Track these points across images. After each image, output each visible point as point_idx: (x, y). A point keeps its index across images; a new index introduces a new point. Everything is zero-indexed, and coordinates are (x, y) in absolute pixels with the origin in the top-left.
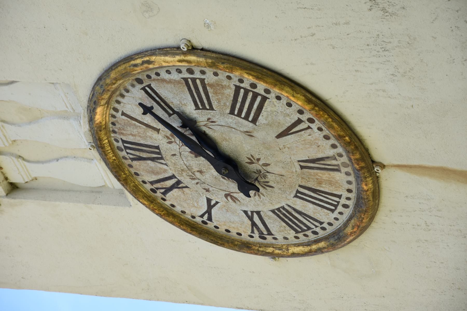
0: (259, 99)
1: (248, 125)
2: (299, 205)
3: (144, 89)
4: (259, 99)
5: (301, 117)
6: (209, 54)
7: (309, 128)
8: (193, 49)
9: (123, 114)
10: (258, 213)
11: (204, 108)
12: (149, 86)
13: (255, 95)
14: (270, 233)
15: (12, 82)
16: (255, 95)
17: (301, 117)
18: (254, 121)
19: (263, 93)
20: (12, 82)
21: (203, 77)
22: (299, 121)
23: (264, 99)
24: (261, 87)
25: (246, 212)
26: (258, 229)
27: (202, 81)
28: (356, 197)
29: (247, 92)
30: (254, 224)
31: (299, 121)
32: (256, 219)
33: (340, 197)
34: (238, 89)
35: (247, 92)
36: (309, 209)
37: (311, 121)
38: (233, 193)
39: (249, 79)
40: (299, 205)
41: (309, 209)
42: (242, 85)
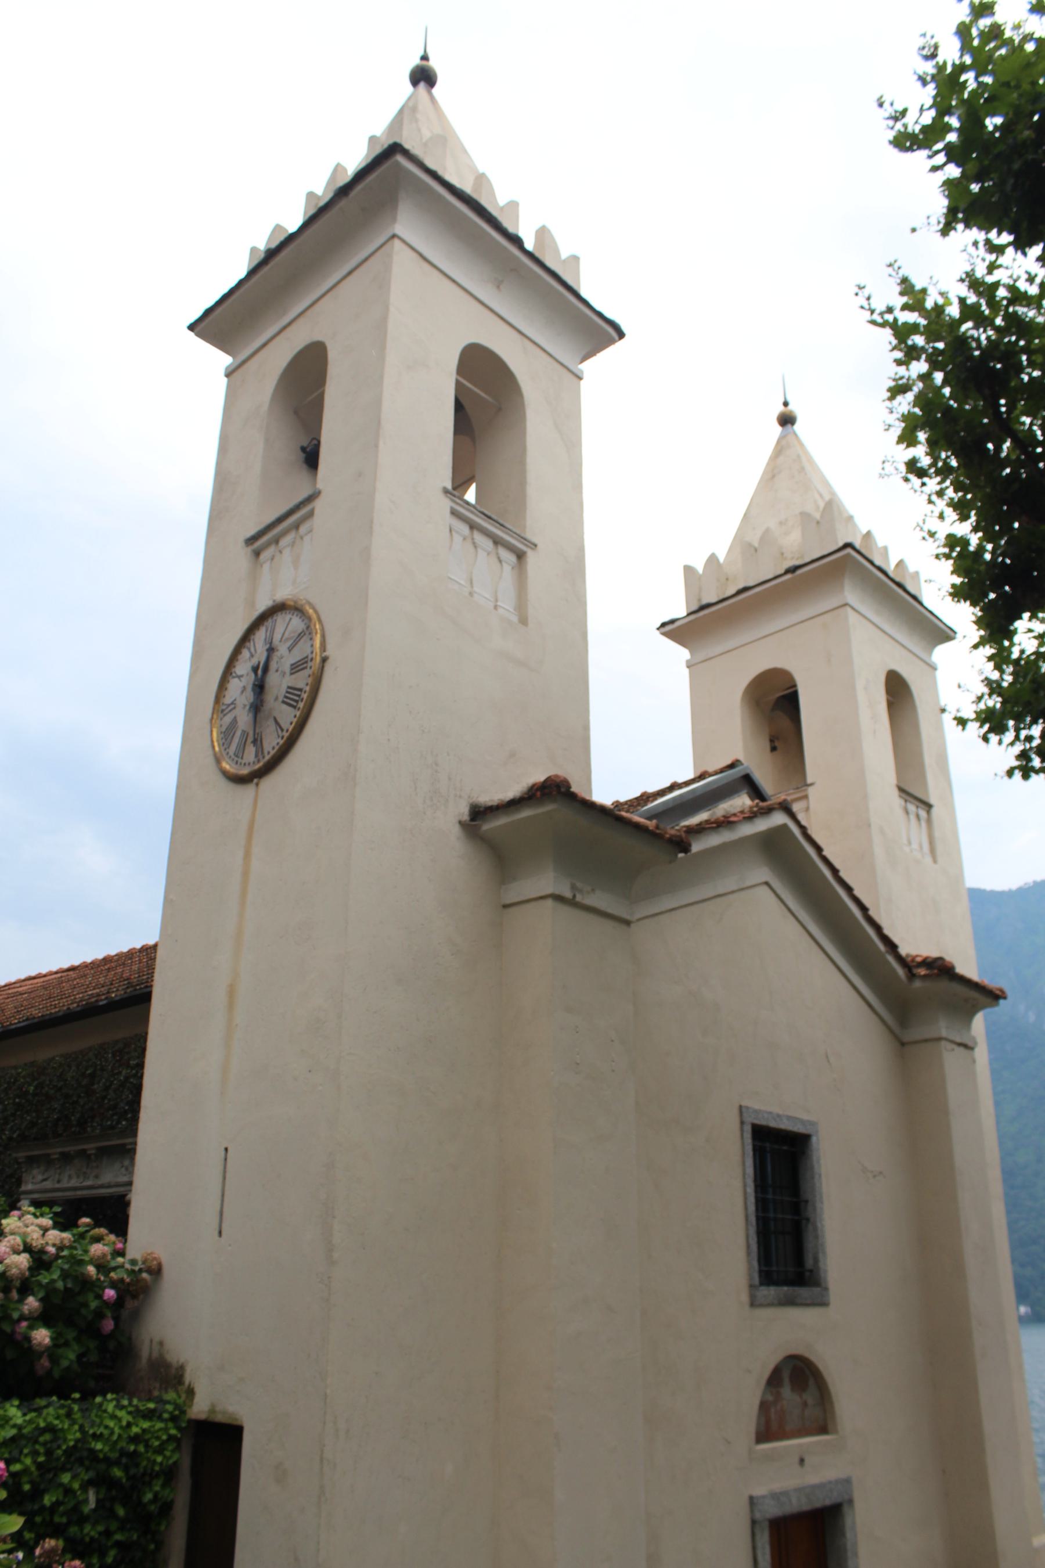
0: (295, 704)
1: (281, 699)
2: (238, 733)
3: (303, 631)
4: (295, 704)
5: (285, 731)
6: (320, 671)
7: (279, 736)
8: (324, 660)
9: (291, 619)
10: (234, 708)
11: (292, 669)
12: (305, 634)
13: (297, 701)
14: (225, 715)
15: (426, 29)
16: (297, 701)
17: (285, 731)
18: (284, 702)
19: (298, 706)
20: (426, 29)
21: (308, 668)
22: (282, 730)
23: (294, 707)
24: (301, 705)
25: (235, 700)
26: (227, 708)
27: (306, 668)
28: (71, 1149)
29: (299, 696)
30: (229, 705)
31: (282, 730)
32: (233, 706)
33: (242, 758)
34: (300, 690)
35: (299, 696)
36: (236, 740)
37: (283, 737)
38: (513, 613)
39: (305, 696)
40: (238, 733)
41: (236, 740)
42: (303, 693)
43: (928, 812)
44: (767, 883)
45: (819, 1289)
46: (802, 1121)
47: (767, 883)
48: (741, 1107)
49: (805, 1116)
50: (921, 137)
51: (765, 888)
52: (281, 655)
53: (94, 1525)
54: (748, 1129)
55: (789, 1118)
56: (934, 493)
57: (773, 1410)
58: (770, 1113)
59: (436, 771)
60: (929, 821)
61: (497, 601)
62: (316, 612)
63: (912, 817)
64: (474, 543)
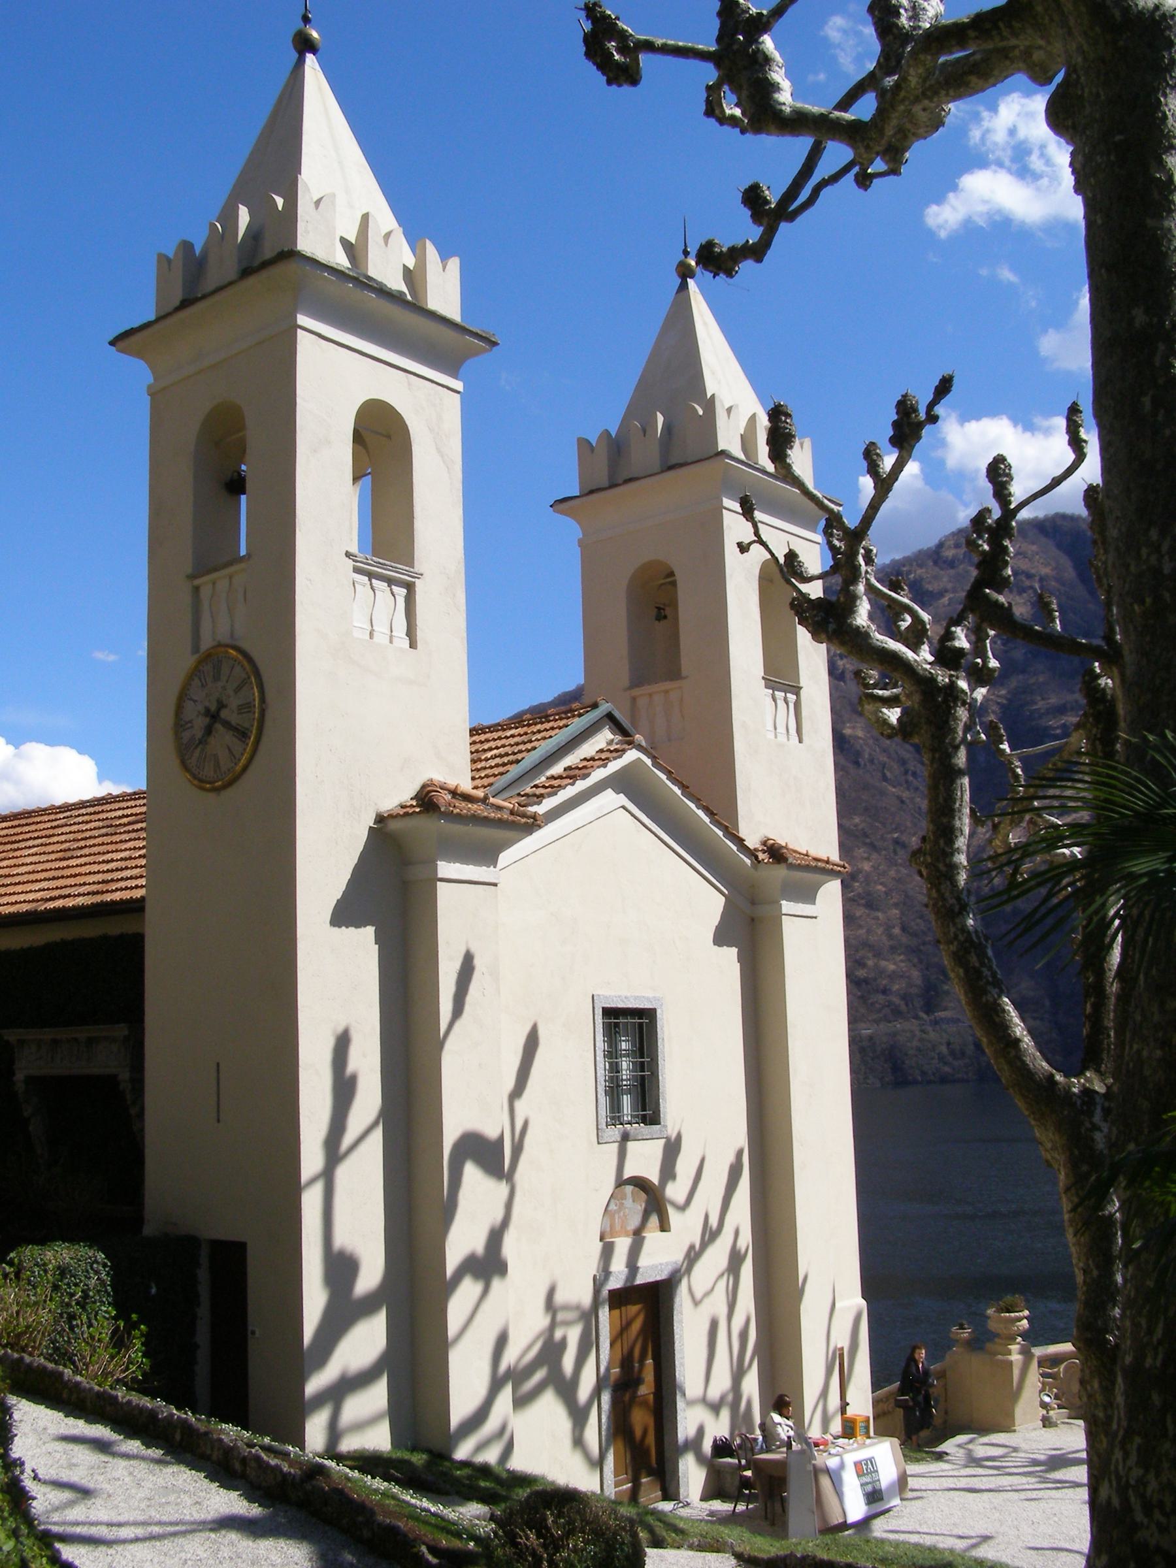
31: (235, 758)
43: (797, 694)
44: (623, 807)
45: (658, 1126)
46: (648, 999)
47: (623, 807)
48: (593, 996)
49: (650, 994)
50: (984, 272)
51: (621, 809)
52: (222, 687)
53: (290, 1466)
54: (599, 1012)
55: (636, 998)
56: (975, 828)
57: (617, 1216)
58: (619, 997)
59: (352, 791)
60: (797, 705)
61: (392, 632)
62: (263, 700)
63: (781, 703)
64: (372, 588)
